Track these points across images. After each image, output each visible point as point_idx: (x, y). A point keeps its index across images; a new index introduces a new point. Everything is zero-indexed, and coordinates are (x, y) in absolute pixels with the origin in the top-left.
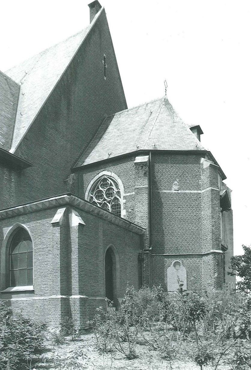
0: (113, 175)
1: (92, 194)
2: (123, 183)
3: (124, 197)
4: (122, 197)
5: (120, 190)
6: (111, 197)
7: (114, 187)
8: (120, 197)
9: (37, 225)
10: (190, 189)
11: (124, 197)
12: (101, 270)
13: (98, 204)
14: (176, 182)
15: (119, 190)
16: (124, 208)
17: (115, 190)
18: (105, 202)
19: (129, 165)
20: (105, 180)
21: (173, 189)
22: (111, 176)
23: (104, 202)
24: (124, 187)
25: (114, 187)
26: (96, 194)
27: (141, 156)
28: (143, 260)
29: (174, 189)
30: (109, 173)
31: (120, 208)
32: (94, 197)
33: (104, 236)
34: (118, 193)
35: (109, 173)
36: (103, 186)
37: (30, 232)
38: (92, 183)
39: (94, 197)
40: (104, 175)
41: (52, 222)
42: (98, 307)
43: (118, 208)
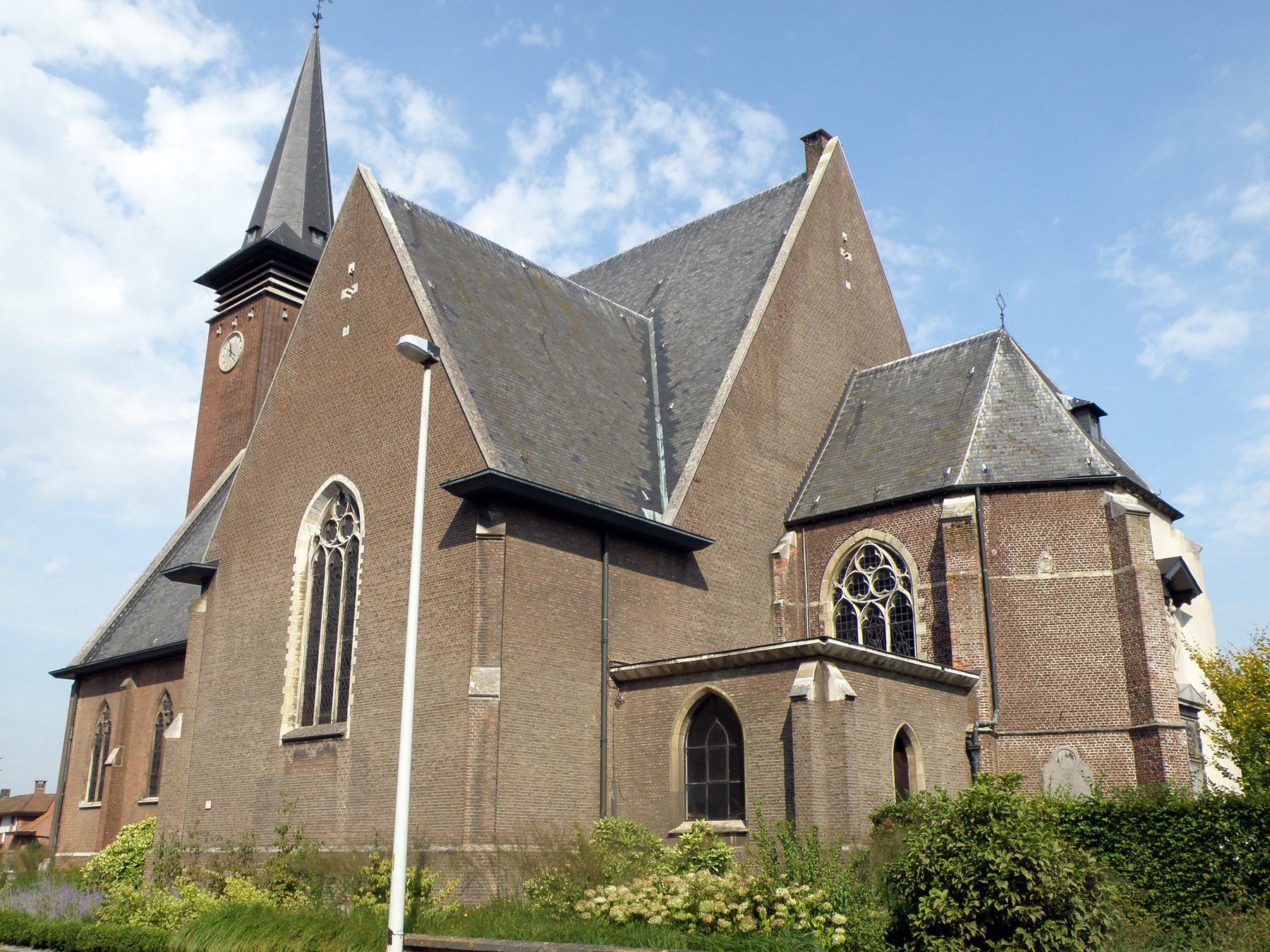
0: (889, 538)
1: (840, 582)
3: (920, 591)
10: (1082, 569)
11: (920, 591)
16: (923, 619)
18: (873, 601)
19: (924, 516)
20: (870, 550)
21: (1040, 571)
25: (894, 567)
26: (848, 581)
28: (978, 750)
29: (1045, 570)
30: (880, 535)
31: (911, 616)
32: (845, 590)
34: (907, 584)
35: (869, 532)
36: (866, 563)
38: (837, 555)
39: (845, 590)
42: (499, 852)
43: (905, 618)
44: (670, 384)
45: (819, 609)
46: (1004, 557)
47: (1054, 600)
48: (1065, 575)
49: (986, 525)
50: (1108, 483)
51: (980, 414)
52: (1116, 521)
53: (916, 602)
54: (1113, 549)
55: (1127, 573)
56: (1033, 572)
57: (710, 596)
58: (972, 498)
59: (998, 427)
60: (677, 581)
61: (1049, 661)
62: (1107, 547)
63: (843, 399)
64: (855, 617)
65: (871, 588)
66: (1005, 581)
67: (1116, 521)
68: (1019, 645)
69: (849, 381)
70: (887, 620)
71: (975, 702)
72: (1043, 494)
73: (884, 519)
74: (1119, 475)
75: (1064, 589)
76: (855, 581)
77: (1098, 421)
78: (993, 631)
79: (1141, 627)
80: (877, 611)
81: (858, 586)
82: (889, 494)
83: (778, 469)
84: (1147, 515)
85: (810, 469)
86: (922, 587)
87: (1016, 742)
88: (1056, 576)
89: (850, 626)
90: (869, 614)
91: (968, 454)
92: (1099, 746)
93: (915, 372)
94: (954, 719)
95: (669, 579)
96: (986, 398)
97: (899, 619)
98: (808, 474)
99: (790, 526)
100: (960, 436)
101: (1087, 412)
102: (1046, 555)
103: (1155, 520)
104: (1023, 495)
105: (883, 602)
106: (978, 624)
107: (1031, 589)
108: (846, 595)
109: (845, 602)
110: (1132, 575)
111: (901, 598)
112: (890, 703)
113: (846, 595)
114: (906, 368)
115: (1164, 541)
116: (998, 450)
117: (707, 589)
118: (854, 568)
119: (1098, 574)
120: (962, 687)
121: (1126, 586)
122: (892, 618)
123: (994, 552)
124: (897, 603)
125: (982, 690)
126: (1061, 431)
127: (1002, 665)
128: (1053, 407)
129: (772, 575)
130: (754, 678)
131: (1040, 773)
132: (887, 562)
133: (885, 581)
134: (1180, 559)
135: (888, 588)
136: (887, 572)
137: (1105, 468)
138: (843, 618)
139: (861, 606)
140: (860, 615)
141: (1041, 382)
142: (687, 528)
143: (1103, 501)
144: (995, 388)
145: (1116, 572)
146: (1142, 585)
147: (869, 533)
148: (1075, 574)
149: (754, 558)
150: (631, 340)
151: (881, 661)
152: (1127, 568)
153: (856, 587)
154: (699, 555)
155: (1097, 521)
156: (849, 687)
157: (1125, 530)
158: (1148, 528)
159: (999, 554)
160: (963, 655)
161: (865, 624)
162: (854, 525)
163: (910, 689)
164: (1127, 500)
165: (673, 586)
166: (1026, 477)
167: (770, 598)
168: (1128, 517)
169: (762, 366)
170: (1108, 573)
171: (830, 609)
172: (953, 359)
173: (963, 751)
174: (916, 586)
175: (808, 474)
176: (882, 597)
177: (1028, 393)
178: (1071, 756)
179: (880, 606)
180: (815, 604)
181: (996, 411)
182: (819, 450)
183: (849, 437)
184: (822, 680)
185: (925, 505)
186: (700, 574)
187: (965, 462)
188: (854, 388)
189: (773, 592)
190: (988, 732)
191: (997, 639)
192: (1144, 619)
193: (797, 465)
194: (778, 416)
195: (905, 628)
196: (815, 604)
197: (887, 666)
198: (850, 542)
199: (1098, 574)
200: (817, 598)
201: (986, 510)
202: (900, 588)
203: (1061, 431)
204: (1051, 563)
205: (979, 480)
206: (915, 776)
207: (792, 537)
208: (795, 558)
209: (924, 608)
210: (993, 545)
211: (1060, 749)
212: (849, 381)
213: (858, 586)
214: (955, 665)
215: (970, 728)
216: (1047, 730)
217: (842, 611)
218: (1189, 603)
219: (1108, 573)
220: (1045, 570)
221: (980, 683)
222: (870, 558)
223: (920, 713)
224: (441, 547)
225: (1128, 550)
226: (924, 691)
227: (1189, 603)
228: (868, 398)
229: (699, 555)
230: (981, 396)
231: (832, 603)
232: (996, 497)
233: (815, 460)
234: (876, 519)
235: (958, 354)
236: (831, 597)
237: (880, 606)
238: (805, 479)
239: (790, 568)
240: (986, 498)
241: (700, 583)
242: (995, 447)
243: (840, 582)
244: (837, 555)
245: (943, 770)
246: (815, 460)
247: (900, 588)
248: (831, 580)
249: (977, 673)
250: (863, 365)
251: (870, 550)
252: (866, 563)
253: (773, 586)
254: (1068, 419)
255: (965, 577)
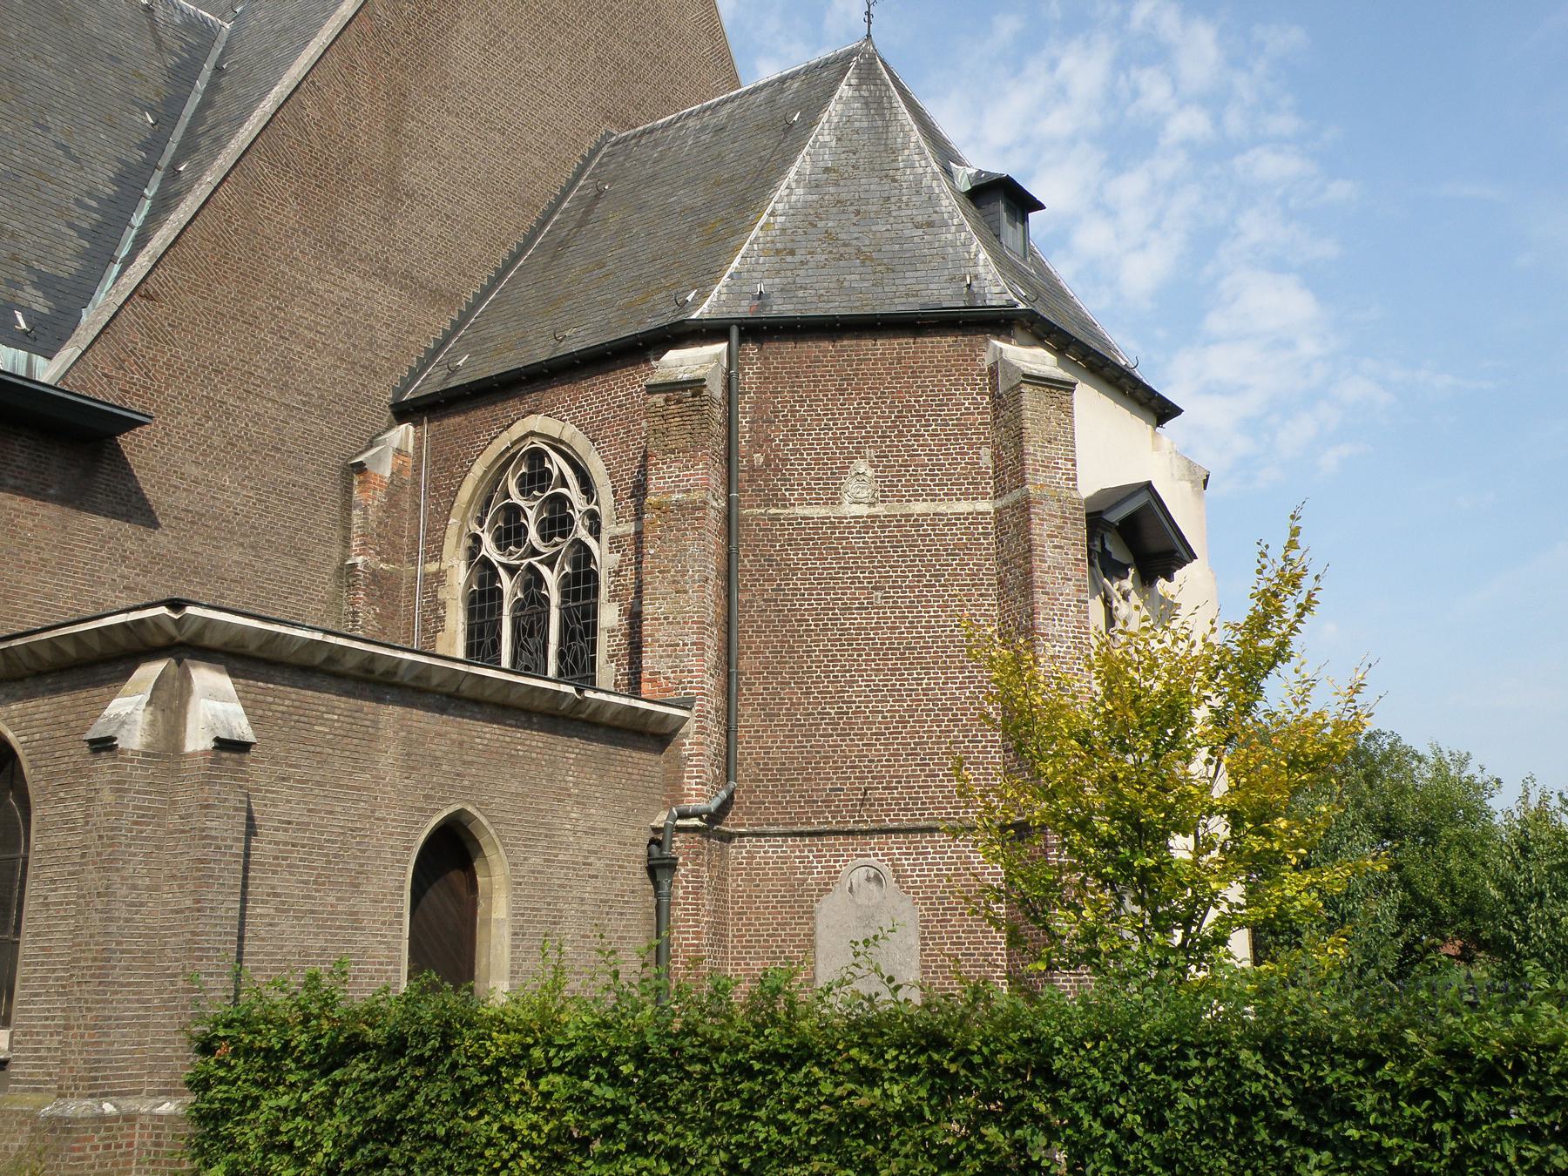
0: (568, 432)
1: (481, 524)
2: (610, 475)
4: (604, 536)
5: (597, 504)
6: (557, 539)
7: (574, 493)
8: (598, 539)
9: (58, 734)
10: (934, 497)
12: (381, 943)
13: (501, 570)
14: (862, 466)
15: (592, 506)
16: (614, 596)
17: (577, 506)
18: (533, 560)
19: (625, 385)
20: (537, 456)
21: (847, 499)
22: (562, 442)
23: (526, 562)
24: (615, 493)
25: (574, 493)
26: (494, 521)
27: (693, 345)
28: (671, 866)
29: (857, 499)
30: (552, 427)
32: (487, 539)
33: (409, 769)
35: (536, 422)
37: (25, 765)
38: (478, 469)
39: (487, 539)
40: (532, 434)
41: (90, 735)
44: (201, 129)
45: (439, 577)
46: (777, 470)
47: (871, 558)
48: (897, 509)
49: (744, 405)
50: (1001, 322)
51: (782, 191)
52: (1004, 397)
53: (605, 559)
54: (996, 457)
55: (1015, 506)
56: (834, 500)
57: (161, 540)
58: (721, 347)
59: (807, 218)
60: (64, 500)
61: (850, 683)
62: (986, 454)
63: (572, 184)
64: (501, 591)
65: (533, 535)
66: (775, 518)
67: (1004, 397)
68: (791, 651)
69: (593, 153)
70: (555, 598)
71: (680, 763)
72: (867, 344)
73: (561, 394)
74: (1022, 306)
75: (891, 537)
76: (507, 521)
77: (1025, 220)
78: (740, 620)
79: (1031, 616)
80: (540, 580)
81: (511, 532)
82: (578, 340)
83: (386, 299)
84: (1068, 387)
85: (472, 308)
86: (618, 531)
87: (767, 851)
88: (880, 509)
89: (492, 612)
90: (526, 587)
91: (736, 264)
92: (942, 854)
93: (703, 129)
94: (619, 800)
95: (39, 494)
96: (802, 163)
97: (576, 599)
98: (465, 317)
99: (403, 412)
100: (734, 233)
101: (1003, 198)
102: (862, 466)
103: (1089, 401)
104: (827, 345)
105: (550, 562)
106: (702, 601)
107: (825, 535)
108: (489, 549)
109: (486, 563)
110: (1024, 506)
111: (583, 556)
112: (409, 763)
113: (489, 549)
114: (691, 123)
115: (1104, 449)
116: (798, 258)
117: (155, 524)
118: (508, 496)
119: (964, 507)
120: (653, 735)
121: (1014, 527)
122: (565, 595)
123: (759, 459)
124: (576, 564)
125: (697, 742)
126: (930, 224)
127: (752, 691)
128: (926, 181)
129: (347, 506)
130: (65, 699)
131: (811, 915)
132: (565, 484)
133: (557, 521)
134: (1148, 486)
135: (563, 535)
136: (562, 501)
137: (996, 291)
138: (482, 594)
139: (512, 570)
140: (507, 584)
141: (916, 135)
142: (103, 391)
143: (987, 360)
144: (824, 145)
145: (999, 503)
146: (1040, 530)
147: (536, 423)
148: (919, 507)
149: (300, 470)
150: (150, 45)
151: (380, 668)
152: (1017, 493)
153: (508, 533)
154: (126, 441)
155: (971, 402)
156: (244, 721)
157: (1018, 416)
158: (1070, 413)
159: (767, 462)
160: (663, 667)
161: (518, 606)
162: (512, 406)
163: (487, 733)
164: (1038, 360)
165: (50, 512)
166: (838, 307)
167: (336, 551)
168: (1027, 390)
169: (364, 89)
170: (985, 506)
171: (459, 575)
172: (771, 101)
173: (641, 874)
174: (609, 529)
175: (465, 317)
176: (548, 551)
177: (885, 147)
178: (878, 879)
179: (544, 570)
180: (433, 567)
181: (815, 186)
182: (501, 274)
183: (558, 247)
184: (171, 704)
185: (635, 364)
186: (139, 490)
187: (725, 279)
188: (600, 164)
189: (346, 541)
190: (695, 829)
191: (750, 639)
192: (1040, 598)
193: (437, 297)
194: (396, 193)
195: (585, 616)
196: (433, 567)
197: (404, 677)
198: (504, 441)
199: (964, 507)
200: (436, 554)
201: (750, 375)
202: (582, 533)
203: (930, 224)
204: (866, 483)
205: (744, 310)
206: (488, 922)
207: (403, 434)
208: (407, 476)
209: (617, 573)
210: (756, 445)
211: (855, 867)
212: (593, 153)
213: (511, 532)
214: (646, 687)
215: (660, 819)
216: (834, 827)
217: (481, 583)
218: (1169, 578)
219: (985, 506)
220: (857, 499)
221: (691, 726)
222: (536, 478)
223: (514, 786)
224: (155, 524)
225: (1020, 457)
226: (536, 740)
227: (1169, 578)
228: (612, 181)
229: (126, 441)
230: (792, 162)
231: (463, 565)
232: (771, 347)
233: (486, 292)
234: (550, 396)
235: (782, 91)
236: (462, 553)
237: (544, 570)
238: (456, 326)
239: (392, 501)
240: (752, 349)
241: (138, 510)
242: (792, 253)
243: (481, 524)
244: (478, 469)
245: (571, 910)
246: (486, 292)
247: (582, 533)
248: (464, 519)
249: (686, 704)
250: (627, 125)
251: (537, 456)
252: (526, 485)
253: (347, 528)
254: (949, 204)
255: (680, 506)
